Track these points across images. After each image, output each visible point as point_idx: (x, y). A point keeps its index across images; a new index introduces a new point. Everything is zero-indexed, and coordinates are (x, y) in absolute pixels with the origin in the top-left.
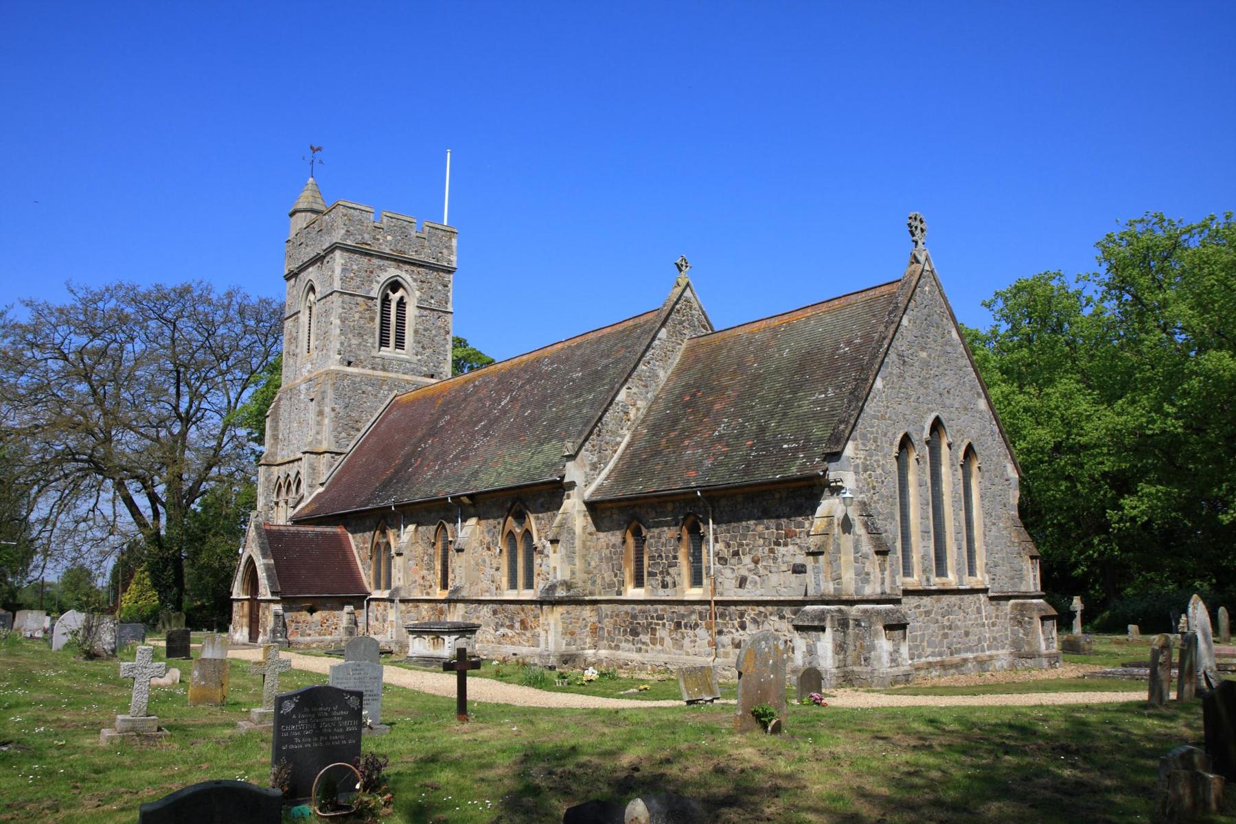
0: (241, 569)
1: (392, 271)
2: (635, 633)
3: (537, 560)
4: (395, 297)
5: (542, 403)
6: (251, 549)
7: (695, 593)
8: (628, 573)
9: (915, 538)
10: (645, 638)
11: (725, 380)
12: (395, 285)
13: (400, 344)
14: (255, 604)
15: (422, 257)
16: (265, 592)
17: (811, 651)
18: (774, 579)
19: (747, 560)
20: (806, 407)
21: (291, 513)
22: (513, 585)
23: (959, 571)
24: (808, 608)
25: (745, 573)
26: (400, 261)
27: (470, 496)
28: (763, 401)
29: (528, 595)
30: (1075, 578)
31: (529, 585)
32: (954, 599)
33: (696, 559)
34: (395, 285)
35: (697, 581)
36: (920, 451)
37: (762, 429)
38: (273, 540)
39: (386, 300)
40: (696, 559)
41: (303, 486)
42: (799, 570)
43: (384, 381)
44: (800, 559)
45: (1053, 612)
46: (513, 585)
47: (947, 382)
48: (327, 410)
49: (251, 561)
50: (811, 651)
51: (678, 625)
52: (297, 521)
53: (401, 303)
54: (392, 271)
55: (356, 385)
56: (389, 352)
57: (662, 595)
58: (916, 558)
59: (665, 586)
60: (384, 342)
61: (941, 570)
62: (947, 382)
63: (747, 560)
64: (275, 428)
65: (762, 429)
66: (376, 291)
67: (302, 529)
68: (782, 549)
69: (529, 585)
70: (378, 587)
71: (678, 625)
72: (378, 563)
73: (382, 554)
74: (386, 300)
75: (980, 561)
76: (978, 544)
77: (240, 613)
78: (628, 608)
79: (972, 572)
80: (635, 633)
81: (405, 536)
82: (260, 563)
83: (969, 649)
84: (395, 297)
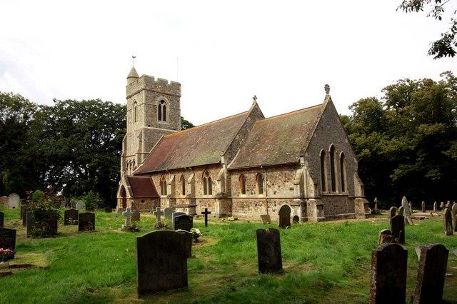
0: (119, 192)
1: (161, 98)
2: (243, 207)
3: (213, 186)
4: (162, 105)
5: (212, 139)
6: (123, 183)
7: (261, 196)
8: (240, 191)
9: (326, 180)
10: (246, 209)
11: (269, 134)
12: (162, 102)
13: (165, 120)
14: (124, 200)
15: (171, 93)
16: (128, 196)
17: (296, 212)
18: (284, 192)
19: (276, 186)
20: (293, 142)
21: (133, 172)
22: (205, 193)
23: (339, 191)
24: (295, 200)
25: (275, 190)
26: (164, 94)
27: (125, 122)
28: (281, 140)
29: (210, 196)
30: (425, 178)
31: (211, 193)
32: (337, 198)
33: (260, 186)
34: (162, 102)
35: (261, 192)
36: (328, 155)
37: (280, 148)
38: (129, 180)
39: (160, 106)
40: (260, 186)
41: (136, 164)
42: (292, 189)
43: (160, 131)
44: (292, 186)
45: (368, 202)
46: (205, 193)
47: (337, 135)
48: (143, 140)
49: (123, 186)
50: (296, 212)
51: (256, 205)
52: (135, 175)
53: (165, 107)
54: (161, 98)
55: (152, 132)
56: (161, 122)
57: (251, 196)
58: (326, 186)
59: (252, 194)
60: (160, 119)
61: (334, 190)
62: (337, 135)
63: (276, 186)
64: (126, 145)
65: (280, 148)
66: (157, 103)
67: (138, 177)
68: (287, 183)
69: (211, 193)
70: (162, 194)
71: (256, 205)
72: (162, 187)
73: (163, 184)
74: (160, 106)
75: (346, 187)
76: (345, 179)
77: (119, 205)
78: (240, 200)
79: (343, 190)
80: (243, 207)
81: (170, 179)
82: (126, 187)
83: (342, 213)
84: (162, 105)
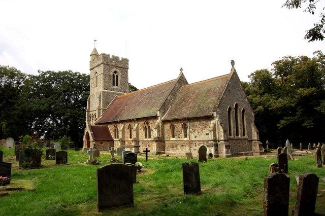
0: (85, 136)
1: (114, 69)
2: (173, 147)
3: (151, 132)
4: (116, 75)
5: (151, 99)
6: (87, 130)
7: (186, 139)
8: (171, 135)
9: (232, 128)
10: (175, 148)
11: (191, 95)
12: (115, 72)
13: (117, 85)
14: (89, 142)
15: (121, 66)
16: (91, 139)
17: (210, 151)
18: (202, 136)
19: (196, 132)
20: (209, 101)
21: (94, 122)
22: (146, 137)
23: (241, 135)
24: (210, 142)
25: (196, 135)
26: (117, 67)
27: (89, 86)
28: (200, 99)
29: (150, 139)
30: (303, 126)
31: (150, 137)
32: (240, 141)
33: (185, 132)
34: (115, 72)
35: (186, 136)
36: (233, 110)
37: (199, 105)
38: (92, 128)
39: (114, 76)
40: (185, 132)
41: (97, 117)
42: (207, 134)
43: (114, 93)
44: (208, 132)
45: (261, 144)
46: (146, 137)
47: (239, 96)
48: (102, 100)
49: (87, 132)
50: (210, 151)
51: (182, 146)
52: (96, 124)
53: (117, 76)
54: (114, 69)
55: (108, 94)
56: (115, 87)
57: (179, 139)
58: (232, 132)
59: (179, 138)
60: (114, 85)
61: (238, 135)
62: (239, 96)
63: (196, 132)
64: (89, 103)
65: (199, 105)
66: (112, 73)
67: (98, 126)
68: (204, 130)
69: (150, 137)
70: (115, 138)
71: (182, 146)
72: (115, 133)
73: (116, 131)
74: (114, 76)
75: (246, 133)
76: (245, 127)
77: (85, 146)
78: (171, 142)
79: (244, 135)
80: (173, 147)
81: (121, 127)
82: (90, 133)
83: (243, 151)
84: (116, 75)
